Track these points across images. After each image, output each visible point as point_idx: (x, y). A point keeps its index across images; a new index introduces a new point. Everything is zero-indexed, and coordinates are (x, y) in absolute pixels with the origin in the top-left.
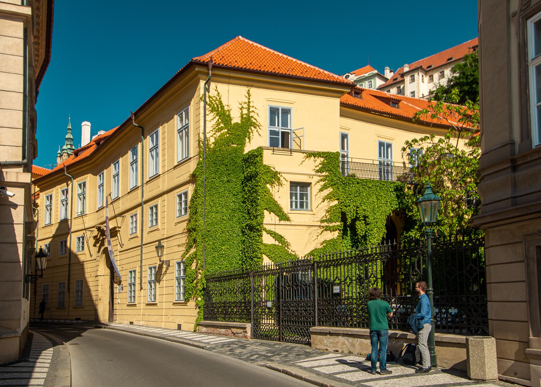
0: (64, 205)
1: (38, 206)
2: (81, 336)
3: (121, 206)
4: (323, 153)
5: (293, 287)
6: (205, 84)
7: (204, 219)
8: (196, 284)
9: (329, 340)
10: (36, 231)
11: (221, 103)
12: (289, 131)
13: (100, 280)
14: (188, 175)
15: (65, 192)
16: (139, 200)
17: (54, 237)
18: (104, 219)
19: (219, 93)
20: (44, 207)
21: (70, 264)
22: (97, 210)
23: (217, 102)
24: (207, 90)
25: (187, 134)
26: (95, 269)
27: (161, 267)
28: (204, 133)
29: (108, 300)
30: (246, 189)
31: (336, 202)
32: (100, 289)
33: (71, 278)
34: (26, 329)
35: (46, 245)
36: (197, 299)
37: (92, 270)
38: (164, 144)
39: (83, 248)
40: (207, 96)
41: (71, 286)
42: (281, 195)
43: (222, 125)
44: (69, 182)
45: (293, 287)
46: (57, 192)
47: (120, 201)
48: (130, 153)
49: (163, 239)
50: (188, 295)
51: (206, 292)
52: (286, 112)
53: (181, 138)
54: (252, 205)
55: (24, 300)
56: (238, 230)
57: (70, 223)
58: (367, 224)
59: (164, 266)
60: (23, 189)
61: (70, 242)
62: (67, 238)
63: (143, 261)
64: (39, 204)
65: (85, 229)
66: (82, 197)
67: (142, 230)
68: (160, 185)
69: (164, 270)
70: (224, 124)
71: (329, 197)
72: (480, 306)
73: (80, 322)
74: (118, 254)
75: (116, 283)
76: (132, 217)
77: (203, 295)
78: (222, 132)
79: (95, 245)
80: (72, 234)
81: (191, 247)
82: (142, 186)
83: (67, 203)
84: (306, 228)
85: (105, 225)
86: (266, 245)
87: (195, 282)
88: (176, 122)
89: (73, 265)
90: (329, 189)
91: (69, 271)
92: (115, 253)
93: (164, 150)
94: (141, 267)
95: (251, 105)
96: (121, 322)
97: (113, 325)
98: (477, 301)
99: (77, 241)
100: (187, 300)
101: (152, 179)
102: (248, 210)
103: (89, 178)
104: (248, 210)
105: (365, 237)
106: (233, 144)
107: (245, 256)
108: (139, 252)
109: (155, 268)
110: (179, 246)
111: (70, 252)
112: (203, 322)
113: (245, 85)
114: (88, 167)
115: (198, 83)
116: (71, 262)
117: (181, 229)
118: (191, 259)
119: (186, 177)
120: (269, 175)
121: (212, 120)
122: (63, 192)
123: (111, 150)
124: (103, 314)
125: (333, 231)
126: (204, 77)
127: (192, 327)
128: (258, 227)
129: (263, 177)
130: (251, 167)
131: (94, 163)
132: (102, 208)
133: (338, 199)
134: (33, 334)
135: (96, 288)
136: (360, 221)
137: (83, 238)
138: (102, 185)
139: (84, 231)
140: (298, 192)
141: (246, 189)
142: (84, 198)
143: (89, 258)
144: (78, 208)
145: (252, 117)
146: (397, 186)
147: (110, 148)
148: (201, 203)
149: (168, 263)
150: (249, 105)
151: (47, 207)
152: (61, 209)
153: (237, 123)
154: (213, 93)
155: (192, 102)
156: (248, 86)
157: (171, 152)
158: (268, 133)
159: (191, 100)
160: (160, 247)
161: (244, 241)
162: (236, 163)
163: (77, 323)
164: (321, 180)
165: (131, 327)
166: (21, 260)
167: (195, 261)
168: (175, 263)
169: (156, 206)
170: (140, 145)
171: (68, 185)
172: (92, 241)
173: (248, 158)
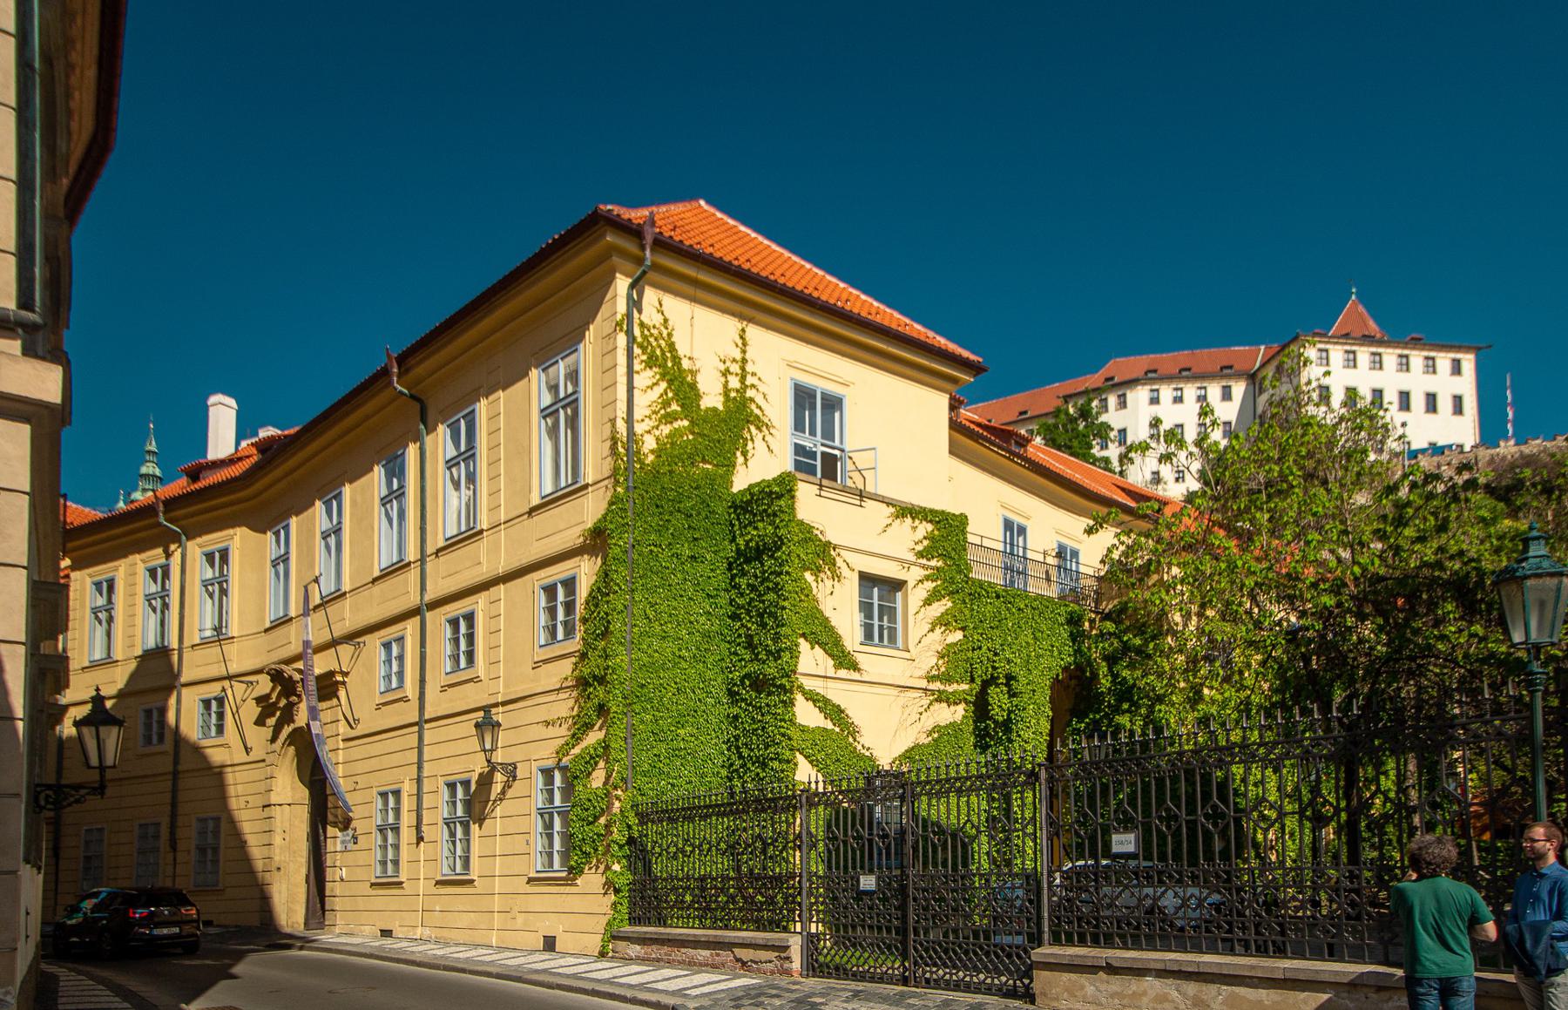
0: (154, 610)
2: (234, 977)
3: (348, 616)
4: (932, 511)
5: (845, 843)
6: (632, 286)
7: (629, 653)
8: (607, 826)
9: (1103, 987)
11: (672, 347)
12: (837, 452)
13: (278, 817)
14: (578, 530)
15: (159, 574)
16: (413, 600)
18: (295, 648)
19: (666, 320)
20: (88, 611)
21: (175, 774)
22: (268, 625)
23: (663, 343)
24: (635, 304)
25: (573, 423)
26: (262, 787)
27: (486, 781)
28: (629, 420)
29: (304, 871)
30: (743, 582)
31: (959, 635)
34: (33, 968)
36: (608, 868)
37: (251, 788)
38: (493, 447)
39: (220, 729)
40: (636, 321)
41: (180, 833)
42: (840, 604)
43: (675, 407)
44: (173, 547)
45: (845, 843)
46: (132, 572)
47: (347, 603)
48: (378, 472)
49: (496, 705)
50: (576, 856)
51: (638, 853)
52: (833, 404)
53: (553, 432)
54: (764, 625)
55: (26, 871)
56: (718, 688)
57: (175, 658)
58: (1012, 694)
59: (499, 777)
60: (27, 428)
63: (425, 765)
65: (230, 678)
66: (219, 588)
67: (422, 681)
68: (484, 559)
69: (497, 788)
70: (682, 406)
71: (942, 622)
74: (341, 745)
75: (335, 825)
76: (387, 646)
77: (628, 857)
78: (676, 425)
79: (260, 722)
80: (184, 691)
81: (588, 726)
82: (422, 560)
83: (166, 606)
84: (895, 691)
85: (300, 665)
86: (803, 729)
87: (602, 820)
88: (535, 388)
89: (190, 777)
90: (944, 601)
91: (175, 791)
92: (330, 744)
93: (493, 463)
94: (419, 780)
95: (749, 368)
96: (355, 926)
97: (326, 937)
99: (202, 710)
100: (574, 872)
101: (452, 544)
102: (750, 637)
103: (239, 539)
104: (750, 637)
105: (1006, 726)
106: (704, 461)
107: (741, 757)
108: (413, 740)
109: (466, 784)
110: (547, 723)
111: (178, 738)
112: (628, 929)
113: (733, 314)
115: (609, 281)
116: (180, 768)
117: (555, 680)
118: (590, 761)
119: (572, 537)
120: (812, 548)
121: (649, 391)
122: (152, 572)
124: (289, 903)
125: (956, 704)
126: (629, 266)
127: (594, 942)
128: (784, 681)
129: (794, 550)
130: (760, 525)
132: (285, 621)
133: (963, 629)
134: (54, 978)
135: (265, 839)
136: (997, 685)
137: (221, 701)
138: (284, 559)
139: (226, 683)
140: (876, 602)
141: (743, 582)
142: (224, 592)
143: (241, 756)
144: (202, 616)
145: (752, 400)
146: (1071, 613)
148: (620, 607)
149: (511, 772)
150: (743, 369)
152: (145, 619)
153: (715, 409)
154: (649, 315)
155: (591, 334)
156: (741, 317)
157: (513, 476)
158: (790, 450)
159: (586, 326)
160: (487, 725)
161: (736, 717)
162: (713, 512)
164: (927, 578)
165: (387, 942)
166: (19, 711)
167: (602, 764)
168: (534, 769)
169: (470, 618)
170: (412, 451)
171: (168, 555)
172: (251, 711)
173: (749, 502)
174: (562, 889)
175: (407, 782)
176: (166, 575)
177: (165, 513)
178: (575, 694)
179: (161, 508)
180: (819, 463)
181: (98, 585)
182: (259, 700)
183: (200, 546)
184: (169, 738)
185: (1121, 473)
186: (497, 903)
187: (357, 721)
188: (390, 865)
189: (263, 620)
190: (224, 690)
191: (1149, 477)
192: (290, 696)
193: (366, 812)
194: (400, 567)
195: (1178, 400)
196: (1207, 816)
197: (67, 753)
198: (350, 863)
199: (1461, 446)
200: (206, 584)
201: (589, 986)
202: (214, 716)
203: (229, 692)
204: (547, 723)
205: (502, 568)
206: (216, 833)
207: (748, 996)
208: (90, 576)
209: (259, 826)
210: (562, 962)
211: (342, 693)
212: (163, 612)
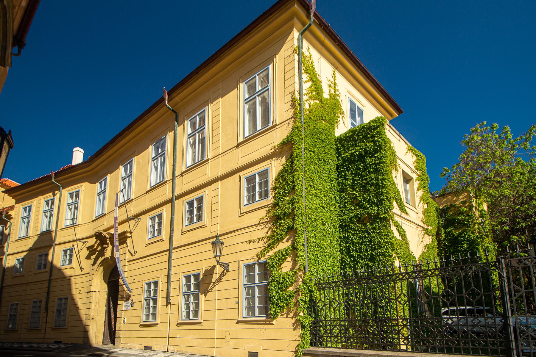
0: (47, 217)
1: (12, 218)
3: (133, 209)
10: (6, 244)
14: (270, 147)
16: (169, 196)
17: (30, 250)
20: (20, 218)
26: (87, 284)
27: (209, 273)
28: (300, 92)
29: (104, 320)
32: (93, 306)
33: (51, 296)
35: (18, 260)
36: (296, 315)
39: (70, 262)
41: (50, 304)
47: (133, 204)
48: (152, 148)
51: (313, 308)
57: (54, 234)
61: (53, 255)
62: (49, 251)
64: (13, 216)
69: (215, 277)
74: (127, 264)
79: (88, 258)
80: (56, 247)
81: (279, 240)
82: (173, 179)
84: (415, 226)
91: (49, 287)
94: (169, 276)
103: (84, 188)
107: (351, 256)
108: (166, 258)
109: (197, 276)
110: (250, 242)
113: (331, 63)
114: (84, 175)
115: (290, 31)
118: (282, 257)
122: (47, 202)
137: (71, 250)
142: (76, 208)
143: (79, 272)
144: (66, 216)
147: (119, 149)
149: (226, 267)
151: (23, 218)
155: (279, 58)
163: (58, 348)
170: (170, 136)
171: (54, 195)
172: (85, 252)
174: (262, 326)
175: (162, 277)
176: (53, 203)
177: (55, 178)
178: (269, 225)
179: (53, 176)
181: (25, 209)
182: (88, 248)
183: (68, 191)
184: (48, 266)
186: (216, 334)
187: (135, 252)
188: (151, 316)
189: (92, 216)
190: (73, 246)
192: (103, 245)
193: (138, 291)
194: (162, 184)
196: (469, 294)
197: (6, 274)
198: (129, 315)
200: (69, 205)
202: (68, 257)
203: (76, 246)
204: (250, 242)
205: (220, 173)
206: (66, 304)
208: (22, 205)
209: (85, 301)
211: (129, 241)
212: (50, 218)
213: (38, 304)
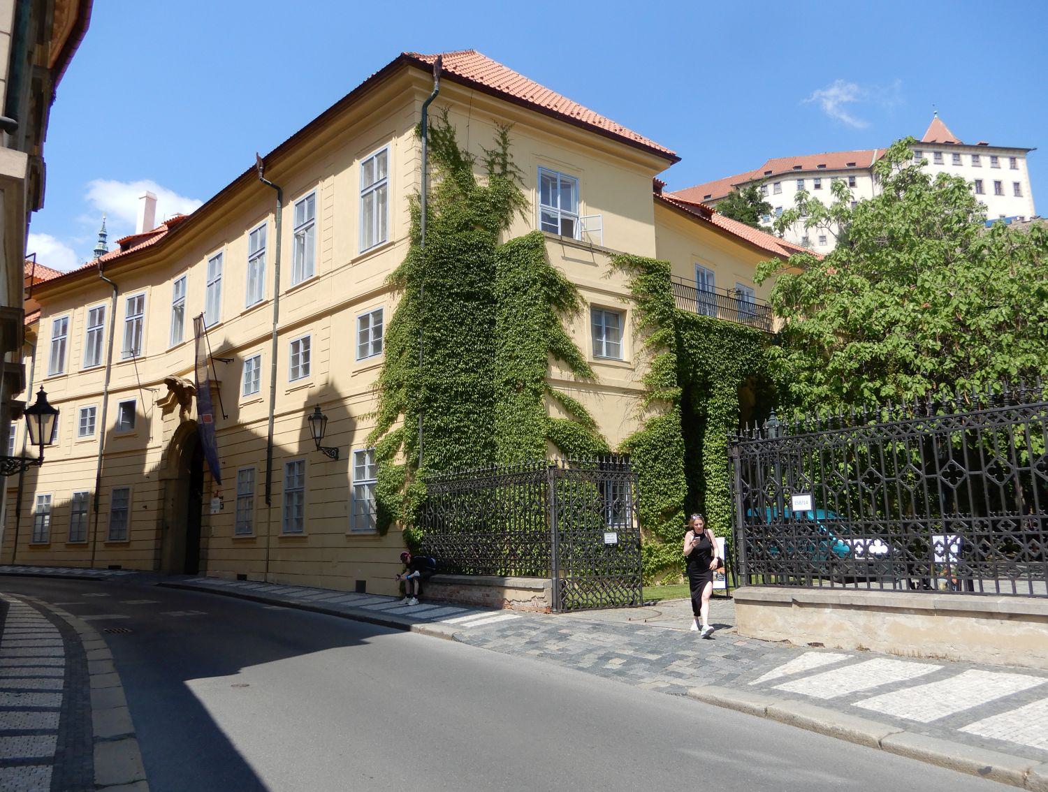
25: (383, 198)
46: (78, 318)
72: (1024, 538)
73: (119, 573)
95: (509, 159)
98: (1017, 529)
123: (209, 228)
131: (164, 258)
165: (243, 585)
169: (306, 341)
180: (559, 225)
185: (781, 237)
191: (800, 240)
195: (818, 186)
199: (1022, 218)
201: (388, 619)
207: (510, 628)
210: (370, 601)
213: (248, 477)
